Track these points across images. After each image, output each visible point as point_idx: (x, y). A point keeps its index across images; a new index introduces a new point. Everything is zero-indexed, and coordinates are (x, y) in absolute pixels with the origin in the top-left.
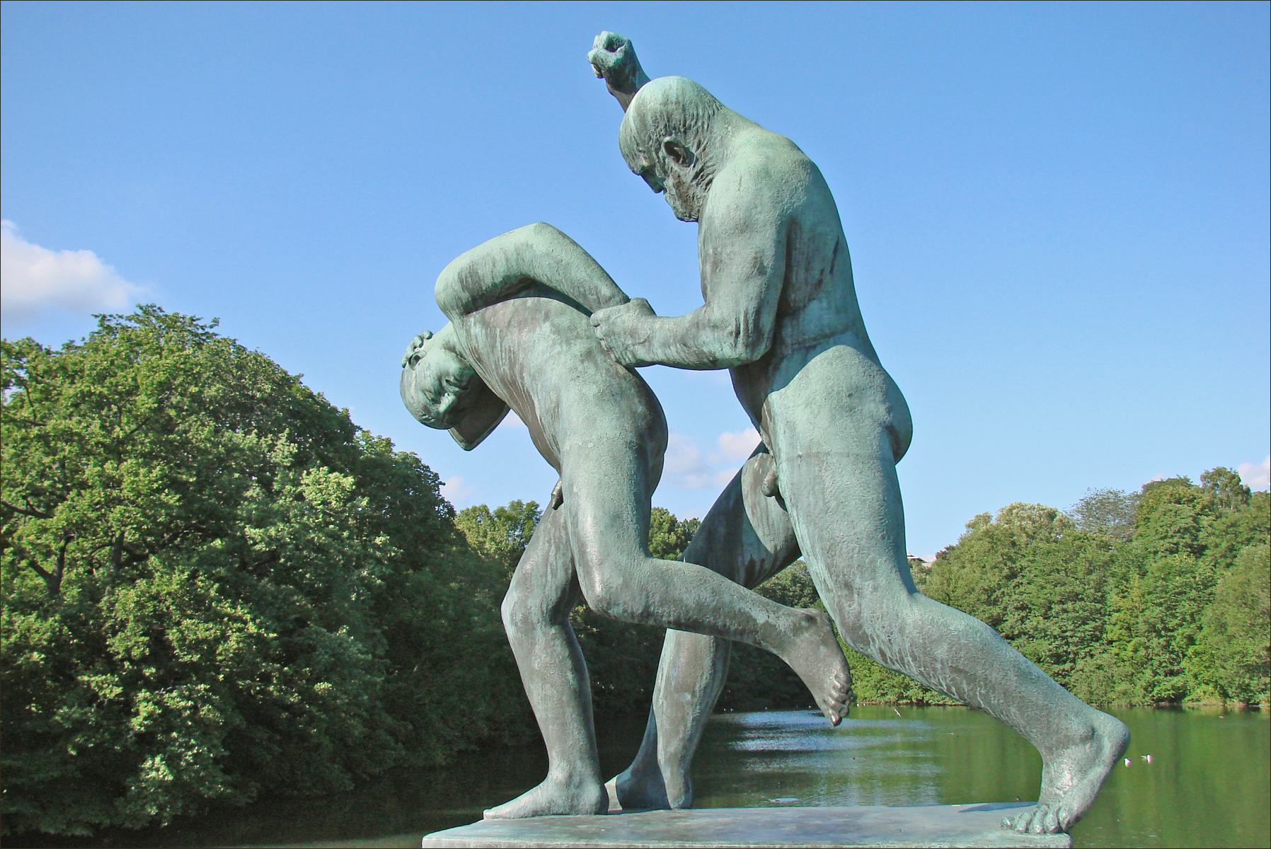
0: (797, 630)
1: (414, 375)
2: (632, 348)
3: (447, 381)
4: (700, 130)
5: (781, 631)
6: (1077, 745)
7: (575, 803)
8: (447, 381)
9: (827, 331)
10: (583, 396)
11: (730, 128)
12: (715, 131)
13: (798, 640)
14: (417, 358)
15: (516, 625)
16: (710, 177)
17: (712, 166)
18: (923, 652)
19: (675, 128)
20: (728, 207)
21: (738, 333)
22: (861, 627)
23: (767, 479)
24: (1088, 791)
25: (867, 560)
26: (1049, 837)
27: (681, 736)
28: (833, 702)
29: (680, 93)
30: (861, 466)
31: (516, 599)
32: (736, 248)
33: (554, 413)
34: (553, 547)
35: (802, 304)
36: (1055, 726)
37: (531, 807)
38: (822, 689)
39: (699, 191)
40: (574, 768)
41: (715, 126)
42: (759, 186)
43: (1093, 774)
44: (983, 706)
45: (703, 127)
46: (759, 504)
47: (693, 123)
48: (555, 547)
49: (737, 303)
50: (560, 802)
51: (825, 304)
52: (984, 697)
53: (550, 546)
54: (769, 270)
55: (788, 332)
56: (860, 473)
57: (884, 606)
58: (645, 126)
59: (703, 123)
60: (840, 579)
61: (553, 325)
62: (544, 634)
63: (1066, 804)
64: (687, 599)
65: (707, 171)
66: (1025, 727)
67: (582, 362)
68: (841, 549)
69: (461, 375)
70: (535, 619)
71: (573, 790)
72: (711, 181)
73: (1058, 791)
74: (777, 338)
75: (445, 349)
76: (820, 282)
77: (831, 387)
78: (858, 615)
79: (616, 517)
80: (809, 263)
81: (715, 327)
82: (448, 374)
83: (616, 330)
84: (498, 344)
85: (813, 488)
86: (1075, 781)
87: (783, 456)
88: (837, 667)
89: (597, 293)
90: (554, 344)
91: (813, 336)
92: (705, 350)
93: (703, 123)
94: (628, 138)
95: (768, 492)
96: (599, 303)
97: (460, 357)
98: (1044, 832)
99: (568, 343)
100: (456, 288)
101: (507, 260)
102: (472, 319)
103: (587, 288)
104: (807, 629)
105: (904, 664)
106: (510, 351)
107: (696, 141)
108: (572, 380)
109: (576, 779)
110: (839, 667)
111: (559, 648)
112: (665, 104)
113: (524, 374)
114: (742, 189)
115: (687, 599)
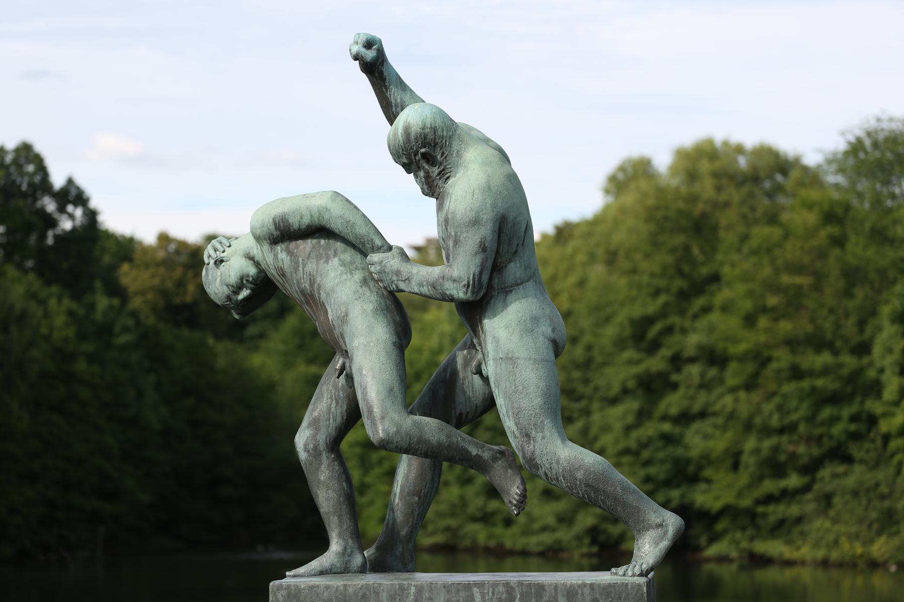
0: (494, 459)
1: (219, 273)
2: (396, 282)
3: (247, 280)
4: (444, 145)
5: (485, 460)
6: (654, 529)
7: (348, 565)
8: (247, 280)
9: (519, 281)
10: (364, 311)
11: (463, 145)
12: (453, 146)
13: (495, 465)
14: (222, 261)
15: (308, 451)
16: (448, 175)
17: (450, 168)
18: (570, 473)
19: (428, 144)
20: (466, 209)
21: (468, 286)
22: (534, 459)
23: (474, 363)
24: (658, 554)
25: (539, 421)
26: (636, 578)
27: (410, 524)
28: (515, 503)
29: (432, 122)
30: (537, 366)
31: (308, 435)
32: (469, 234)
33: (344, 319)
34: (334, 402)
35: (504, 265)
36: (642, 518)
37: (319, 569)
38: (509, 494)
39: (440, 183)
40: (347, 544)
41: (454, 143)
42: (484, 197)
43: (662, 545)
44: (602, 506)
45: (446, 144)
46: (467, 377)
47: (440, 141)
48: (335, 401)
49: (469, 268)
50: (338, 565)
51: (518, 265)
52: (603, 501)
53: (332, 401)
54: (488, 249)
55: (496, 281)
56: (536, 370)
57: (548, 447)
58: (409, 141)
59: (446, 141)
60: (523, 431)
61: (340, 260)
62: (328, 458)
63: (646, 561)
64: (433, 440)
65: (446, 171)
66: (625, 519)
67: (361, 286)
68: (525, 414)
69: (258, 277)
70: (322, 449)
71: (347, 558)
72: (448, 177)
73: (642, 554)
74: (490, 285)
75: (246, 257)
76: (516, 251)
77: (521, 317)
78: (533, 453)
79: (391, 390)
80: (510, 241)
81: (455, 281)
82: (248, 276)
83: (387, 270)
84: (301, 269)
85: (509, 377)
86: (652, 548)
87: (491, 357)
88: (518, 481)
89: (372, 244)
90: (341, 274)
91: (510, 285)
92: (448, 293)
93: (446, 141)
94: (397, 145)
95: (474, 371)
96: (373, 249)
97: (257, 264)
98: (633, 575)
99: (351, 274)
100: (271, 228)
101: (311, 216)
102: (279, 248)
103: (366, 239)
104: (500, 459)
105: (558, 481)
106: (310, 273)
107: (441, 152)
108: (356, 299)
109: (349, 551)
110: (519, 482)
111: (337, 468)
112: (423, 129)
113: (321, 292)
114: (474, 198)
115: (433, 440)
